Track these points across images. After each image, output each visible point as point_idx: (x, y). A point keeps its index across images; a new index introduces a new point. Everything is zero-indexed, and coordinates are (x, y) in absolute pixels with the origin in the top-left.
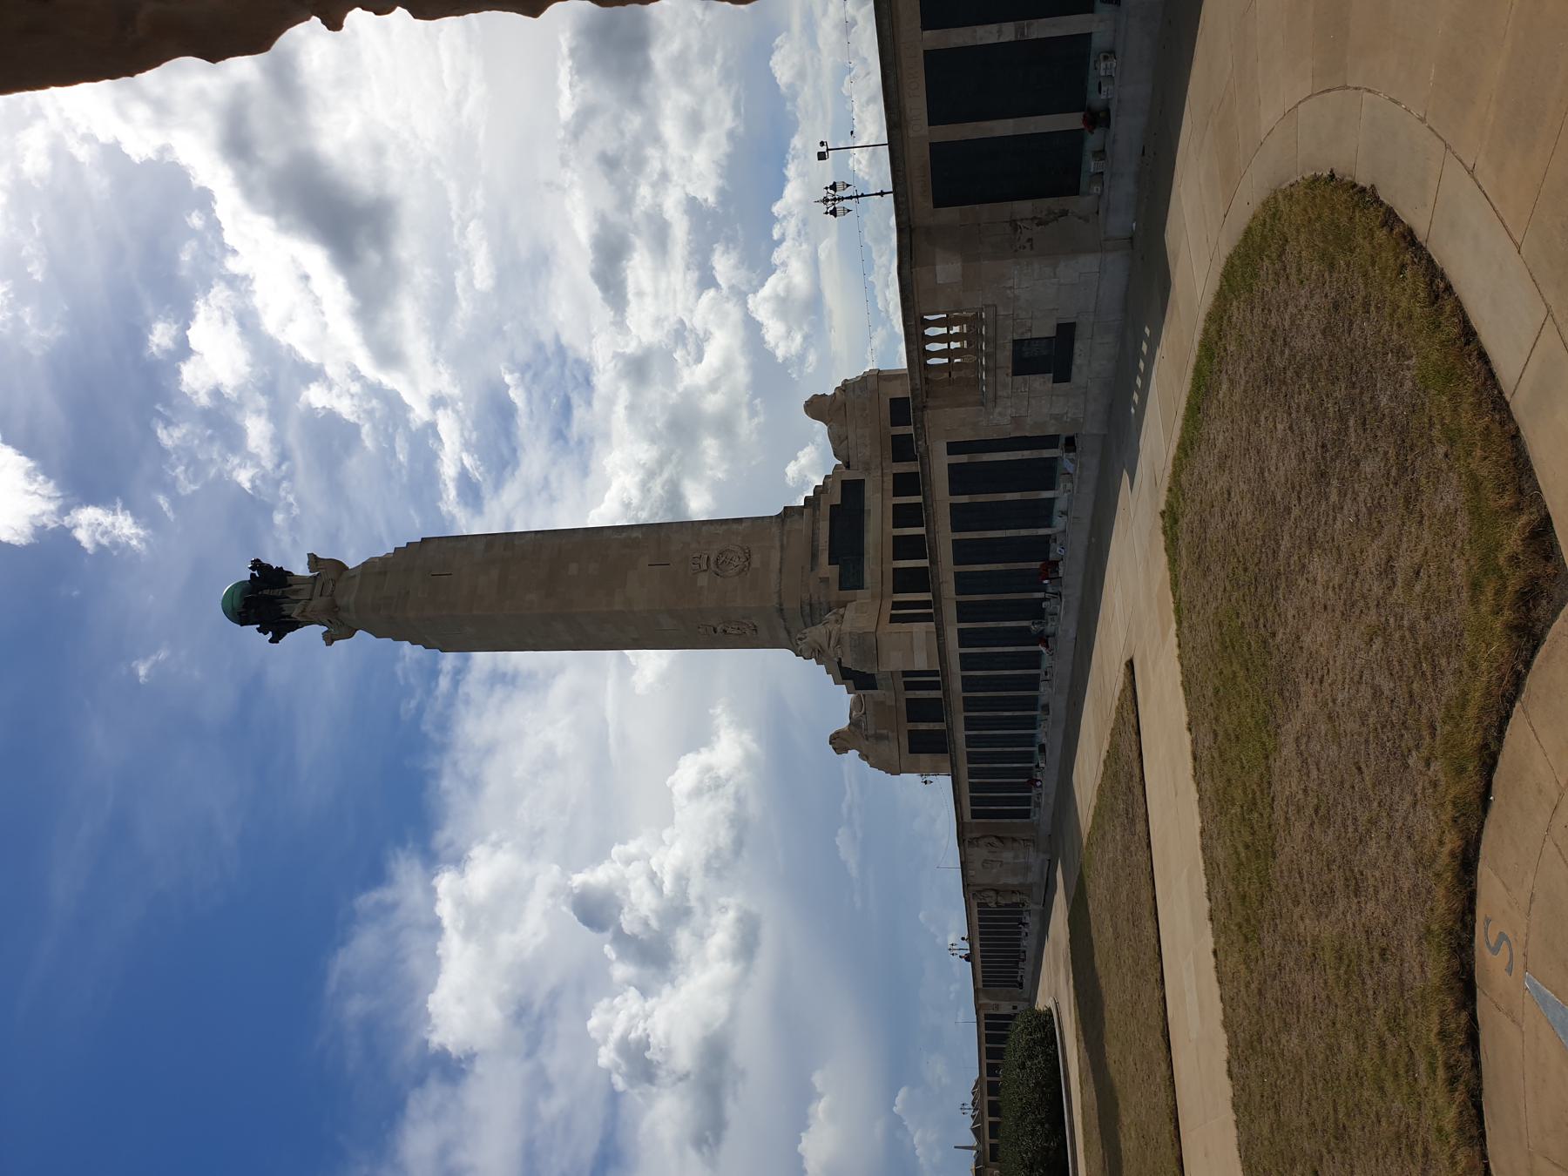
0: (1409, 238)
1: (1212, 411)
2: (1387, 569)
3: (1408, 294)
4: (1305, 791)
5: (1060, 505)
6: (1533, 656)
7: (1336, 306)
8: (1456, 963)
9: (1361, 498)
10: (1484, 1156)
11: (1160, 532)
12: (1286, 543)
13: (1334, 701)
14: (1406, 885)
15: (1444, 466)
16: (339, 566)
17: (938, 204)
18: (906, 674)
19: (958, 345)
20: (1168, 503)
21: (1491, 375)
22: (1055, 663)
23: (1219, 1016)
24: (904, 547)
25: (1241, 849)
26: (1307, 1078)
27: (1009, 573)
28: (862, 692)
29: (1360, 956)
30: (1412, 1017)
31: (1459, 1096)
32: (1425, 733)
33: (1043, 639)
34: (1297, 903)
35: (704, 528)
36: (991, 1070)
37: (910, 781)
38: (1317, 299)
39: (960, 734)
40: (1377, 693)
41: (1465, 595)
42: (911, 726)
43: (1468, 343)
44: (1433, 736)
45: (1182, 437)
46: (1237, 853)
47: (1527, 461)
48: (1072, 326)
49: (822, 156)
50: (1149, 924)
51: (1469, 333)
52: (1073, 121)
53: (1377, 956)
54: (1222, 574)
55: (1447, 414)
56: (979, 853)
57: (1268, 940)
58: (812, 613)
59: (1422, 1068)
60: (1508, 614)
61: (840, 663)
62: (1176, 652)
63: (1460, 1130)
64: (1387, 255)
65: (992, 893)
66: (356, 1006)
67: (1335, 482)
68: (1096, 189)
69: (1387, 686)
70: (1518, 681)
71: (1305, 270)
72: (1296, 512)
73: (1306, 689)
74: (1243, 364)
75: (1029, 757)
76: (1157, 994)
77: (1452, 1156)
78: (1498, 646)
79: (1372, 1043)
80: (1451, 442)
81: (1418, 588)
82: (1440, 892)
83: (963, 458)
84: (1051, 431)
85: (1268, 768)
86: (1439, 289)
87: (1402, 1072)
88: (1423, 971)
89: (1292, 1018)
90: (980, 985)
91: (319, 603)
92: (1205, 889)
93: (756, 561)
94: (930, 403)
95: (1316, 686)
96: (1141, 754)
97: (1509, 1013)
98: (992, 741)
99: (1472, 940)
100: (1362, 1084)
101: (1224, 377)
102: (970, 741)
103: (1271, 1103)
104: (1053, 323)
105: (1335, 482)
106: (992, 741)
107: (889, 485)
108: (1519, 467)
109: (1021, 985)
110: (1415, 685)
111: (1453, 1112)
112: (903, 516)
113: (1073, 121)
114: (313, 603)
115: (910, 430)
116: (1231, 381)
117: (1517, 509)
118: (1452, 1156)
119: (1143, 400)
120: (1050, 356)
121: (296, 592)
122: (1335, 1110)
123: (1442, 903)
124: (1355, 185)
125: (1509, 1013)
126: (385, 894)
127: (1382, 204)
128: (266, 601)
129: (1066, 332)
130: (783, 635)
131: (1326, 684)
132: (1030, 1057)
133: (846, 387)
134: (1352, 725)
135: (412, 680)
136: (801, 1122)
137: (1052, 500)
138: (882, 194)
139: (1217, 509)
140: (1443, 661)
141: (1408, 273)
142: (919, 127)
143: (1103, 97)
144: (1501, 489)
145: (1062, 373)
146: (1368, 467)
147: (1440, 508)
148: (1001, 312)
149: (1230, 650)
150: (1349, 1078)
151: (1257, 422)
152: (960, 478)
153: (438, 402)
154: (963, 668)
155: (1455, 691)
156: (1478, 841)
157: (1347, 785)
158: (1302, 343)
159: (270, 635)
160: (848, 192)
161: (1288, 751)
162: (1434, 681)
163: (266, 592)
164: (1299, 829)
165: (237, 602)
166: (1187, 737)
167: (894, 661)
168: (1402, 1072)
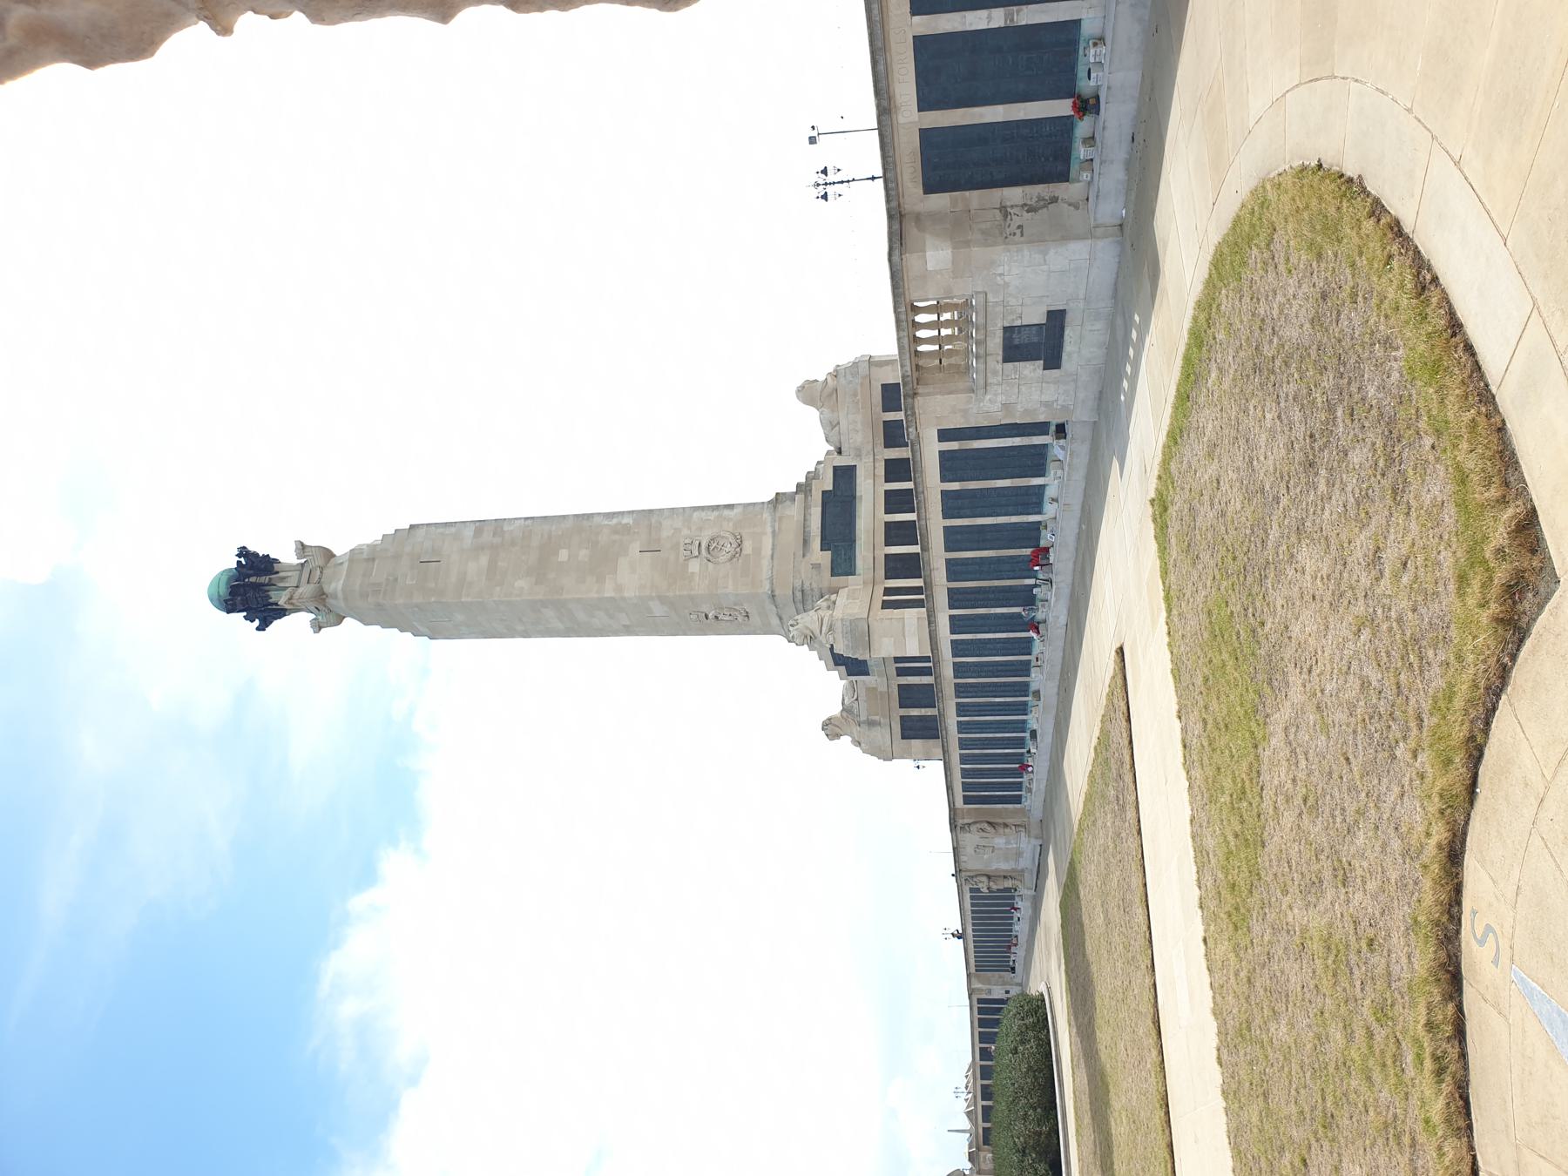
0: (1396, 229)
1: (1202, 400)
2: (1375, 558)
3: (1395, 285)
4: (1294, 780)
5: (1050, 492)
7: (1324, 296)
8: (1442, 954)
9: (1349, 489)
10: (1471, 1148)
12: (1274, 533)
13: (1322, 691)
14: (1393, 876)
15: (1431, 458)
16: (328, 554)
17: (929, 188)
18: (897, 660)
20: (1159, 492)
21: (1477, 367)
22: (1046, 649)
24: (895, 533)
25: (1231, 838)
27: (999, 560)
28: (854, 678)
29: (1347, 946)
31: (1447, 1087)
32: (1413, 724)
34: (1285, 892)
35: (696, 515)
40: (1365, 684)
41: (1452, 587)
42: (904, 712)
43: (1454, 335)
44: (1420, 727)
47: (1513, 454)
48: (1062, 313)
49: (812, 140)
50: (1140, 911)
51: (1455, 326)
52: (1063, 108)
53: (1364, 946)
55: (1435, 405)
56: (971, 839)
57: (1257, 928)
58: (803, 600)
59: (1409, 1058)
60: (1494, 608)
61: (832, 648)
62: (1167, 639)
63: (1448, 1121)
65: (984, 879)
66: (349, 1009)
67: (1323, 472)
68: (1085, 176)
69: (1374, 676)
70: (1504, 673)
71: (1294, 260)
72: (1284, 501)
73: (1295, 679)
75: (1021, 743)
76: (1148, 981)
77: (1440, 1148)
78: (1485, 638)
79: (1360, 1033)
80: (1438, 433)
81: (1405, 580)
82: (1427, 884)
83: (954, 446)
84: (1042, 418)
86: (1425, 281)
87: (1389, 1062)
89: (1280, 1007)
90: (973, 970)
91: (306, 590)
92: (1195, 877)
93: (748, 547)
94: (921, 390)
96: (1131, 742)
97: (1496, 1006)
99: (1458, 932)
100: (1349, 1074)
101: (1214, 366)
102: (962, 727)
103: (1260, 1091)
104: (1044, 310)
105: (1323, 472)
107: (881, 471)
108: (1506, 459)
109: (1013, 969)
110: (1402, 677)
112: (896, 501)
113: (1063, 108)
115: (900, 416)
116: (1220, 369)
117: (1503, 501)
118: (1440, 1148)
120: (1040, 343)
121: (283, 579)
122: (1324, 1099)
123: (1429, 895)
124: (1342, 176)
125: (1496, 1006)
128: (252, 590)
129: (1057, 319)
130: (775, 621)
132: (1023, 1042)
134: (1340, 716)
137: (1042, 487)
138: (873, 178)
139: (1206, 498)
140: (1430, 653)
141: (1395, 263)
142: (910, 117)
143: (1092, 83)
146: (1357, 457)
147: (1427, 499)
148: (991, 298)
149: (1219, 639)
150: (1337, 1068)
152: (951, 465)
154: (954, 655)
155: (1440, 683)
156: (1465, 834)
157: (1335, 776)
158: (1290, 333)
159: (257, 622)
161: (1277, 741)
162: (1422, 672)
163: (253, 579)
164: (1288, 819)
165: (223, 590)
166: (1177, 725)
167: (885, 648)
168: (1389, 1062)
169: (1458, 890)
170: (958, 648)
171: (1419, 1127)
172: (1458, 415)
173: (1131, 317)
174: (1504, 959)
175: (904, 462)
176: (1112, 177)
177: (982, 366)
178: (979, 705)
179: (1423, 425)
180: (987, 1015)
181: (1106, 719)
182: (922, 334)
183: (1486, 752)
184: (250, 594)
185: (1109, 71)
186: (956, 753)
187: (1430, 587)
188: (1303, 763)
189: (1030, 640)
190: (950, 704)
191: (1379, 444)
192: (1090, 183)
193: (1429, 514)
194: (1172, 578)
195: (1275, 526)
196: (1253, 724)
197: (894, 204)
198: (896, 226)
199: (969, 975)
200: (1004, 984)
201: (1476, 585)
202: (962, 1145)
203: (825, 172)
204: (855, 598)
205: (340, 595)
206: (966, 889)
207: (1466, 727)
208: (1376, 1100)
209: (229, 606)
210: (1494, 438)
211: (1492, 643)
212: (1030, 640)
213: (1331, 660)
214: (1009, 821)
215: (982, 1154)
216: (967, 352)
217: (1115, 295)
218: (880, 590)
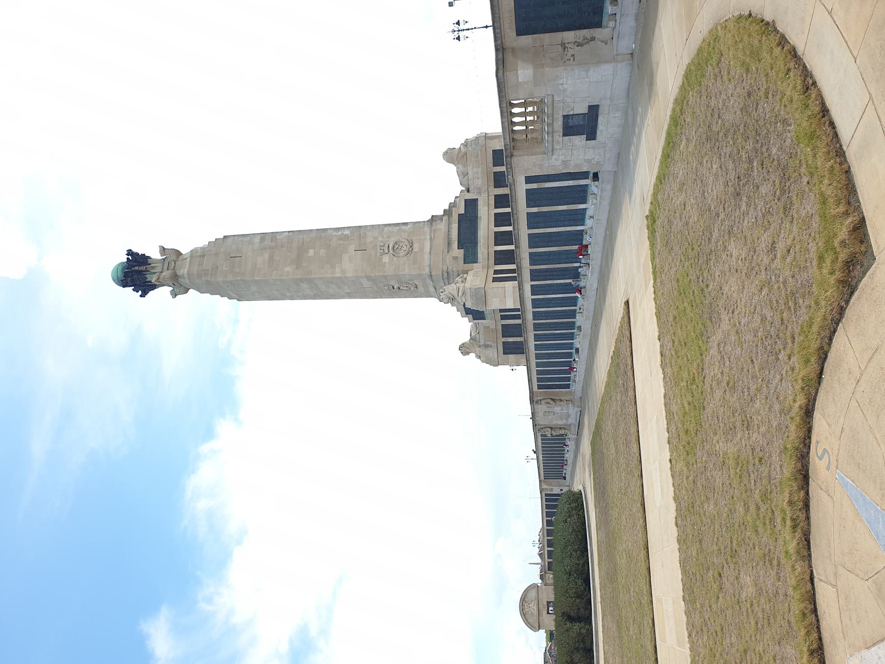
1: (676, 157)
2: (772, 248)
3: (791, 87)
4: (722, 373)
5: (589, 213)
8: (799, 465)
10: (810, 566)
11: (645, 228)
12: (715, 234)
13: (740, 323)
14: (775, 424)
15: (807, 189)
16: (178, 253)
17: (519, 33)
18: (501, 311)
19: (531, 118)
20: (651, 212)
21: (836, 135)
22: (586, 303)
24: (501, 238)
25: (686, 405)
27: (559, 252)
28: (477, 321)
29: (748, 462)
32: (789, 341)
34: (715, 434)
35: (386, 229)
40: (763, 319)
41: (815, 263)
42: (505, 339)
43: (823, 116)
44: (793, 342)
47: (854, 186)
50: (635, 445)
51: (825, 111)
53: (757, 462)
54: (680, 252)
55: (810, 158)
56: (541, 408)
57: (699, 454)
58: (448, 277)
59: (779, 520)
60: (838, 275)
62: (653, 296)
63: (798, 552)
64: (780, 64)
65: (549, 429)
67: (744, 199)
68: (612, 24)
69: (768, 314)
70: (842, 311)
72: (722, 216)
73: (724, 316)
75: (570, 355)
76: (639, 484)
77: (793, 566)
78: (832, 292)
79: (752, 508)
80: (812, 174)
81: (788, 260)
82: (793, 427)
83: (534, 186)
84: (585, 169)
86: (809, 84)
87: (768, 522)
89: (710, 495)
90: (542, 478)
91: (166, 274)
92: (666, 427)
93: (416, 247)
96: (632, 353)
97: (827, 491)
99: (808, 453)
102: (537, 347)
104: (587, 105)
105: (744, 199)
107: (492, 202)
108: (849, 189)
109: (565, 478)
111: (795, 543)
112: (501, 219)
115: (503, 169)
116: (687, 139)
117: (846, 214)
118: (793, 566)
119: (637, 151)
120: (584, 125)
122: (732, 542)
123: (794, 432)
124: (763, 21)
125: (827, 491)
127: (778, 32)
128: (136, 274)
129: (594, 110)
130: (432, 290)
131: (736, 313)
132: (569, 517)
134: (749, 337)
137: (585, 209)
138: (487, 27)
139: (678, 214)
140: (801, 301)
141: (791, 74)
146: (763, 190)
147: (803, 213)
148: (556, 98)
149: (683, 295)
150: (739, 526)
151: (701, 164)
152: (533, 198)
154: (533, 307)
156: (815, 400)
157: (745, 370)
158: (729, 117)
159: (140, 293)
161: (714, 351)
162: (795, 311)
163: (136, 268)
164: (718, 394)
165: (120, 275)
166: (658, 344)
168: (768, 522)
169: (810, 430)
170: (535, 304)
171: (782, 556)
174: (833, 467)
177: (550, 139)
180: (550, 502)
183: (829, 355)
186: (533, 361)
188: (728, 363)
191: (777, 182)
192: (614, 28)
195: (716, 230)
196: (700, 342)
197: (499, 42)
198: (500, 56)
199: (540, 481)
200: (559, 486)
201: (828, 261)
202: (537, 569)
203: (458, 23)
204: (477, 277)
205: (186, 276)
208: (760, 542)
210: (843, 177)
213: (745, 306)
214: (562, 398)
216: (542, 129)
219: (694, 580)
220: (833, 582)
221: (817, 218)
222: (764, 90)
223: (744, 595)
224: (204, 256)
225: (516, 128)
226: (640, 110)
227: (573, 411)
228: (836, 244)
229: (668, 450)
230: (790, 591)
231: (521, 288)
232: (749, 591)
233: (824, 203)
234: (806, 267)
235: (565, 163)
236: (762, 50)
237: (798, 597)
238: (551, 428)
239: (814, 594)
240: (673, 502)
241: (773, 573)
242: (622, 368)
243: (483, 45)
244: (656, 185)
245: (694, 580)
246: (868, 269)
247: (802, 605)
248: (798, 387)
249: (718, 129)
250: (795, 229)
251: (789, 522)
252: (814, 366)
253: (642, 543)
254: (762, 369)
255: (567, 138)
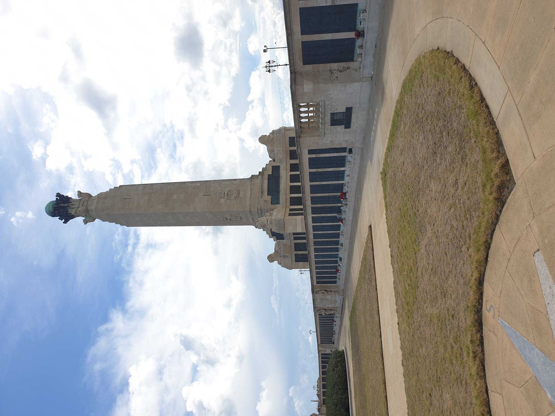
0: (464, 68)
1: (398, 135)
2: (456, 183)
3: (463, 87)
4: (428, 264)
5: (347, 173)
6: (502, 209)
7: (439, 94)
8: (476, 317)
9: (447, 160)
10: (486, 383)
11: (380, 179)
12: (422, 179)
13: (438, 231)
14: (461, 292)
15: (474, 145)
16: (89, 196)
17: (305, 63)
18: (294, 234)
19: (312, 114)
20: (384, 169)
21: (490, 113)
22: (345, 229)
23: (399, 345)
24: (294, 190)
25: (407, 286)
26: (428, 363)
27: (329, 197)
29: (445, 318)
30: (462, 337)
31: (477, 362)
32: (468, 239)
33: (341, 220)
34: (425, 303)
35: (223, 182)
36: (323, 373)
37: (296, 271)
38: (433, 92)
39: (313, 254)
40: (452, 227)
41: (481, 190)
42: (296, 252)
43: (482, 102)
44: (470, 239)
45: (388, 145)
46: (406, 288)
47: (501, 141)
48: (351, 108)
49: (265, 51)
50: (377, 317)
51: (483, 99)
52: (352, 35)
53: (451, 317)
54: (401, 192)
55: (476, 127)
56: (319, 296)
57: (416, 317)
58: (261, 213)
59: (465, 354)
60: (494, 195)
61: (271, 230)
62: (386, 220)
63: (477, 374)
64: (456, 74)
65: (324, 310)
66: (98, 367)
67: (439, 155)
68: (359, 59)
69: (455, 224)
70: (497, 217)
71: (429, 82)
72: (426, 167)
73: (429, 228)
74: (408, 117)
75: (336, 262)
76: (379, 341)
77: (475, 383)
78: (491, 205)
79: (449, 347)
80: (477, 137)
81: (465, 189)
82: (471, 293)
83: (314, 156)
84: (344, 146)
85: (416, 257)
86: (473, 84)
87: (458, 356)
88: (466, 321)
89: (423, 343)
90: (320, 343)
91: (81, 209)
92: (395, 302)
93: (242, 194)
94: (302, 135)
95: (432, 227)
96: (374, 258)
97: (494, 332)
98: (323, 256)
99: (481, 309)
100: (445, 362)
101: (402, 122)
102: (316, 256)
103: (416, 373)
104: (345, 107)
105: (439, 155)
106: (323, 256)
107: (289, 168)
108: (499, 143)
109: (333, 343)
110: (464, 223)
111: (475, 367)
112: (294, 178)
113: (352, 35)
114: (79, 209)
115: (295, 148)
116: (404, 124)
117: (498, 158)
118: (475, 383)
119: (375, 134)
120: (343, 119)
122: (437, 373)
123: (472, 296)
124: (445, 51)
125: (494, 332)
126: (108, 326)
127: (454, 57)
128: (62, 208)
129: (349, 110)
130: (251, 220)
131: (435, 225)
132: (336, 367)
133: (273, 132)
134: (443, 239)
135: (118, 248)
136: (257, 399)
137: (344, 171)
138: (286, 65)
139: (399, 169)
140: (474, 213)
141: (463, 79)
142: (299, 37)
143: (362, 26)
144: (493, 152)
145: (348, 126)
146: (449, 149)
147: (473, 160)
148: (326, 103)
149: (403, 218)
150: (441, 361)
151: (413, 137)
152: (313, 163)
153: (133, 162)
154: (314, 231)
155: (477, 223)
156: (484, 274)
157: (442, 260)
158: (428, 108)
159: (63, 220)
160: (274, 64)
161: (423, 251)
162: (471, 220)
163: (62, 205)
164: (426, 277)
165: (51, 209)
166: (389, 250)
167: (290, 229)
168: (458, 356)
169: (482, 294)
170: (315, 228)
171: (468, 377)
172: (483, 129)
173: (375, 110)
174: (496, 316)
175: (297, 165)
176: (369, 60)
177: (323, 127)
178: (322, 248)
179: (472, 134)
180: (324, 359)
181: (365, 251)
182: (302, 115)
183: (491, 245)
184: (61, 210)
185: (367, 22)
186: (314, 266)
187: (474, 191)
188: (431, 257)
189: (340, 225)
190: (312, 248)
191: (457, 143)
192: (361, 62)
193: (473, 165)
194: (388, 198)
195: (423, 176)
196: (415, 246)
197: (293, 68)
198: (293, 76)
199: (318, 345)
200: (330, 348)
201: (488, 187)
202: (316, 405)
204: (279, 212)
205: (94, 210)
206: (317, 314)
207: (485, 237)
208: (454, 370)
209: (53, 214)
210: (495, 136)
211: (494, 207)
212: (340, 225)
213: (441, 220)
215: (322, 408)
216: (318, 121)
217: (369, 103)
218: (288, 210)
219: (414, 401)
220: (500, 392)
221: (481, 163)
222: (452, 100)
223: (445, 408)
224: (106, 198)
225: (303, 120)
226: (377, 110)
227: (338, 298)
228: (492, 176)
229: (396, 317)
230: (474, 401)
231: (306, 219)
232: (449, 403)
233: (484, 152)
234: (476, 193)
235: (332, 142)
236: (446, 69)
237: (479, 403)
238: (325, 310)
239: (489, 401)
240: (400, 350)
241: (463, 390)
242: (368, 267)
243: (283, 74)
244: (386, 153)
245: (414, 401)
246: (512, 190)
247: (482, 408)
248: (474, 267)
249: (422, 115)
250: (468, 170)
251: (471, 354)
252: (483, 253)
253: (382, 380)
254: (452, 258)
255: (333, 127)
